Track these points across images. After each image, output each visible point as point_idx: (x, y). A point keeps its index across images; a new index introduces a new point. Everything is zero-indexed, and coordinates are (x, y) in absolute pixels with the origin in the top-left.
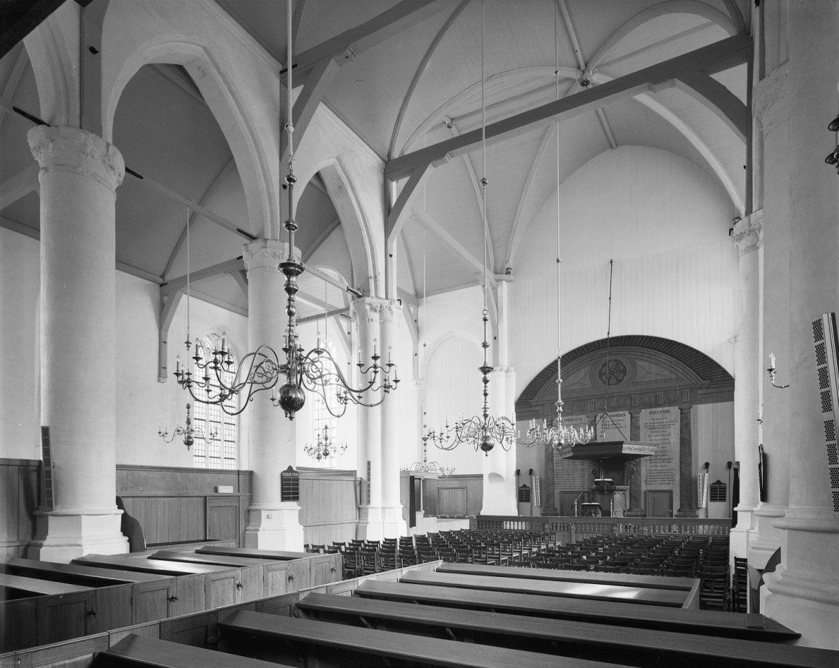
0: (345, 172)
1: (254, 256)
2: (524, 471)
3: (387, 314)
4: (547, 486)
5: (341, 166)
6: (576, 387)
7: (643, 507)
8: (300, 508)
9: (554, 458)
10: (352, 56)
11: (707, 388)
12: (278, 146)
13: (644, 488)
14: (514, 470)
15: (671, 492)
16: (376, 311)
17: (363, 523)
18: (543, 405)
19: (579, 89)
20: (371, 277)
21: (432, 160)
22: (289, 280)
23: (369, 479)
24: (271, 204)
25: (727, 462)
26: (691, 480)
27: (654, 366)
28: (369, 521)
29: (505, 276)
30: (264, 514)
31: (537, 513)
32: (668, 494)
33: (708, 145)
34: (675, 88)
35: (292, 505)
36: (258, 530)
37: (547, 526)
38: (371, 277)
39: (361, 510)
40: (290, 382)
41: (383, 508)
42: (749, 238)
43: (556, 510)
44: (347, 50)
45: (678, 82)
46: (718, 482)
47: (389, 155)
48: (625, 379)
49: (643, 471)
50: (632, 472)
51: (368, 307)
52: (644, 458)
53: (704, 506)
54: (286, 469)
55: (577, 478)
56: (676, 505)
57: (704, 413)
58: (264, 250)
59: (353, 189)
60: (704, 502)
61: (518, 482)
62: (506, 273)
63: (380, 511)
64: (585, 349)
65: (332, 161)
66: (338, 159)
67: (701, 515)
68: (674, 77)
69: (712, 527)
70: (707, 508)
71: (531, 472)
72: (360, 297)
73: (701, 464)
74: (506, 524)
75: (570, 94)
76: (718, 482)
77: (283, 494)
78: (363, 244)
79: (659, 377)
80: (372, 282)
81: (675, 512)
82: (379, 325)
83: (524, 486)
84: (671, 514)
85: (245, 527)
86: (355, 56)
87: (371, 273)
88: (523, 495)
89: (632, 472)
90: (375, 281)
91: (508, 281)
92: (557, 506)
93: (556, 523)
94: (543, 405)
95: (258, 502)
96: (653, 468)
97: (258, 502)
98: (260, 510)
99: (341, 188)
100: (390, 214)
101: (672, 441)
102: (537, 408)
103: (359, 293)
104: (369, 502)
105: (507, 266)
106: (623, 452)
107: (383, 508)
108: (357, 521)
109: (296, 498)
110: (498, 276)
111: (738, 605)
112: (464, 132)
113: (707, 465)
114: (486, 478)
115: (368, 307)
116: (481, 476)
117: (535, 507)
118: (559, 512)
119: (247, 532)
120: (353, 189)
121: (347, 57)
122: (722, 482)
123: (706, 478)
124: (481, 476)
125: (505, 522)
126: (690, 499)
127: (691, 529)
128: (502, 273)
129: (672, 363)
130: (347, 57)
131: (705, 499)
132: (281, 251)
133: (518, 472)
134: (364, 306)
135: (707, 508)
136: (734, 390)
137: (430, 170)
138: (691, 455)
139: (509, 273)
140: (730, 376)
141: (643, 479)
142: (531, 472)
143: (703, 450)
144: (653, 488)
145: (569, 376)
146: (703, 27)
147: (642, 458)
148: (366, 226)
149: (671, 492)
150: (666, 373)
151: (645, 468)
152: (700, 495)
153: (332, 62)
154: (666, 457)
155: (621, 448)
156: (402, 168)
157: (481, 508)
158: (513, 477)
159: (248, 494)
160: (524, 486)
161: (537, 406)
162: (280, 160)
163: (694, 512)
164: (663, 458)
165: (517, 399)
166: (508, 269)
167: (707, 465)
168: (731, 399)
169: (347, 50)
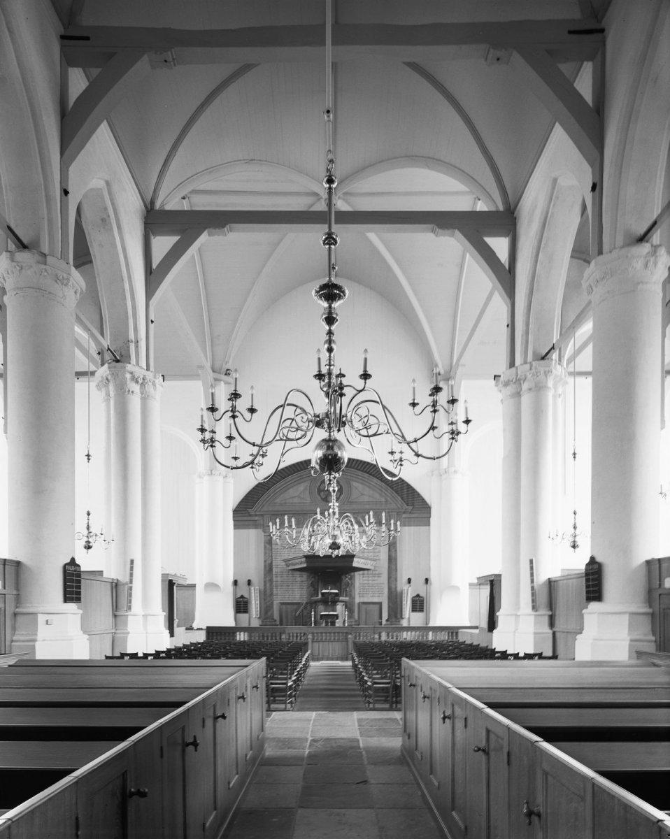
0: (113, 204)
1: (23, 271)
2: (242, 582)
3: (150, 388)
4: (266, 596)
5: (110, 193)
6: (296, 500)
7: (356, 617)
8: (81, 612)
9: (274, 569)
10: (172, 63)
11: (410, 513)
12: (60, 137)
13: (357, 600)
14: (231, 580)
15: (380, 604)
16: (137, 382)
17: (120, 633)
18: (262, 515)
19: (321, 206)
20: (132, 342)
21: (210, 227)
22: (330, 307)
23: (131, 581)
24: (49, 209)
25: (424, 578)
26: (397, 593)
27: (367, 489)
28: (129, 630)
29: (223, 377)
30: (41, 619)
31: (255, 623)
32: (378, 606)
33: (419, 300)
34: (452, 239)
35: (72, 606)
36: (35, 641)
37: (283, 636)
38: (132, 342)
39: (118, 619)
40: (330, 436)
41: (145, 616)
42: (514, 386)
43: (276, 621)
44: (169, 53)
45: (457, 232)
46: (418, 596)
47: (152, 202)
48: (319, 497)
49: (357, 584)
50: (348, 585)
51: (128, 376)
52: (361, 572)
53: (407, 616)
54: (68, 561)
55: (296, 591)
56: (385, 616)
57: (408, 535)
58: (43, 267)
59: (119, 227)
60: (408, 613)
61: (235, 593)
62: (226, 374)
63: (141, 618)
64: (301, 466)
65: (101, 184)
66: (108, 183)
67: (404, 623)
68: (455, 228)
69: (413, 633)
70: (409, 618)
71: (249, 582)
72: (118, 361)
73: (405, 580)
74: (240, 635)
75: (312, 209)
76: (418, 596)
77: (65, 593)
78: (125, 299)
79: (371, 499)
80: (132, 346)
81: (384, 622)
82: (140, 400)
83: (242, 597)
84: (381, 624)
85: (12, 638)
86: (175, 65)
87: (132, 336)
88: (241, 606)
89: (348, 585)
90: (137, 347)
91: (226, 383)
92: (276, 616)
93: (297, 633)
94: (262, 515)
95: (31, 603)
96: (366, 582)
97: (31, 603)
98: (35, 614)
99: (105, 221)
100: (154, 276)
101: (381, 558)
102: (257, 518)
103: (117, 357)
104: (129, 608)
105: (228, 367)
106: (354, 565)
107: (145, 616)
108: (114, 631)
109: (78, 600)
110: (217, 376)
111: (396, 706)
112: (193, 209)
113: (409, 580)
114: (199, 590)
115: (128, 376)
116: (193, 586)
117: (254, 617)
118: (278, 623)
119: (13, 644)
120: (119, 227)
121: (166, 61)
122: (421, 595)
123: (409, 591)
124: (193, 586)
125: (238, 633)
126: (396, 612)
127: (392, 636)
128: (220, 373)
129: (382, 487)
130: (166, 61)
131: (408, 610)
132: (65, 276)
133: (235, 583)
134: (124, 373)
135: (409, 618)
136: (430, 517)
137: (204, 238)
138: (396, 571)
139: (229, 374)
140: (427, 504)
141: (357, 592)
142: (249, 582)
143: (406, 568)
144: (366, 600)
145: (288, 489)
146: (462, 193)
147: (356, 573)
148: (130, 278)
149: (380, 604)
150: (377, 496)
151: (358, 579)
152: (404, 603)
153: (145, 58)
154: (377, 572)
155: (352, 562)
156: (174, 225)
157: (193, 620)
158: (230, 588)
159: (15, 592)
160: (242, 597)
161: (256, 515)
162: (61, 157)
163: (399, 622)
164: (374, 572)
165: (235, 507)
166: (227, 370)
167: (409, 580)
168: (428, 524)
169: (169, 53)
